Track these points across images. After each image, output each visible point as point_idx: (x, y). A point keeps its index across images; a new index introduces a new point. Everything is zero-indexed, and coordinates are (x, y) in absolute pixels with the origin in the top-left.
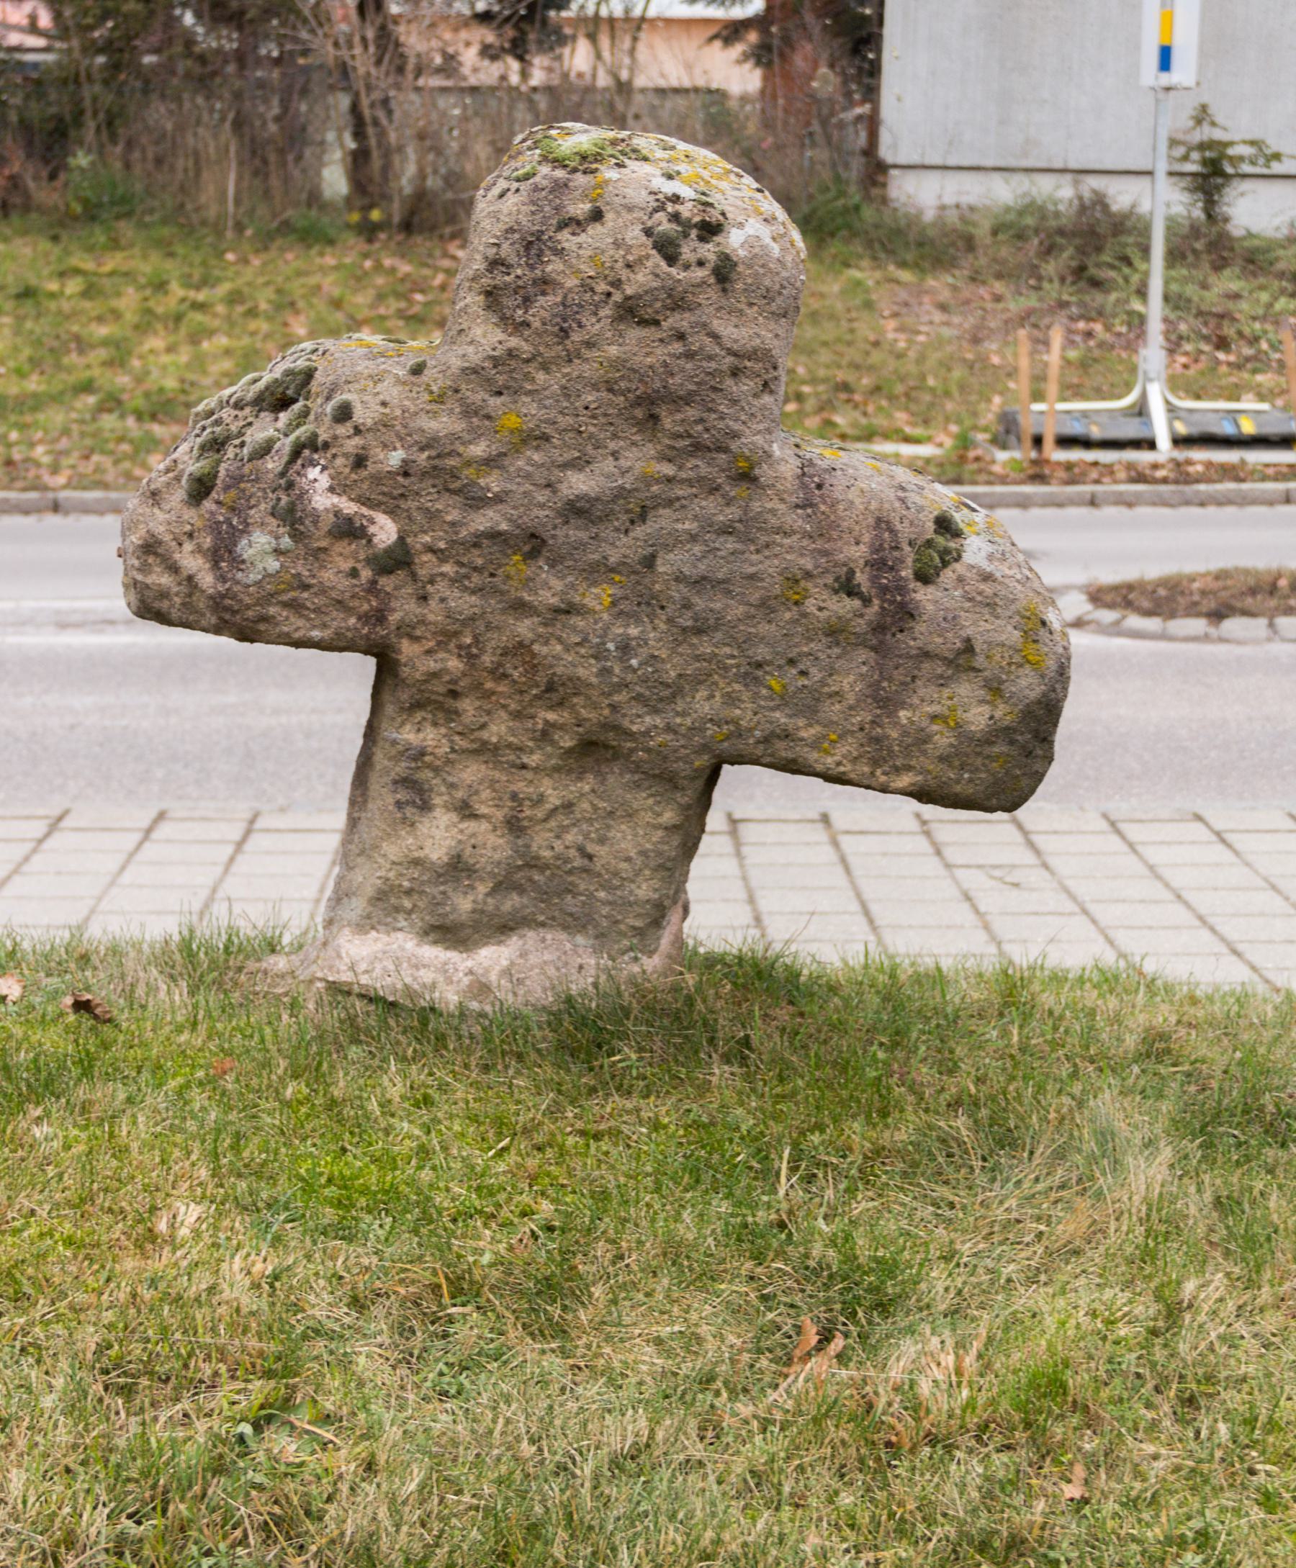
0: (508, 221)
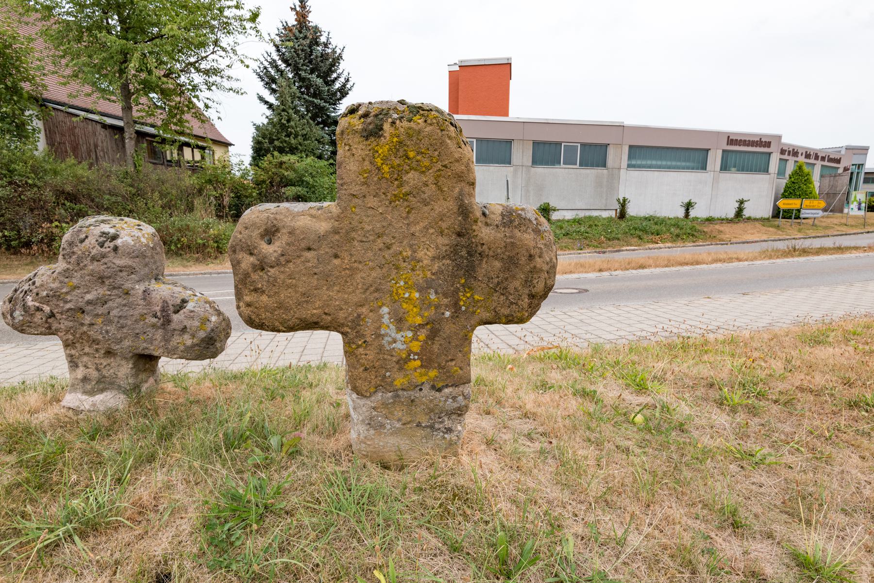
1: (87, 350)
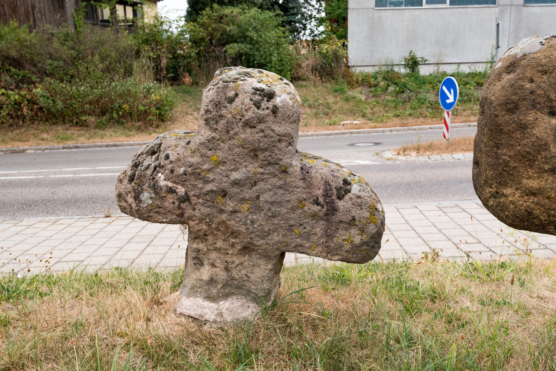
0: (211, 98)
1: (220, 244)
